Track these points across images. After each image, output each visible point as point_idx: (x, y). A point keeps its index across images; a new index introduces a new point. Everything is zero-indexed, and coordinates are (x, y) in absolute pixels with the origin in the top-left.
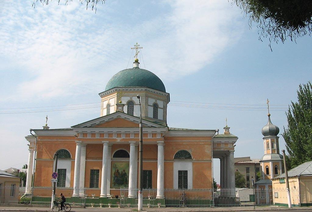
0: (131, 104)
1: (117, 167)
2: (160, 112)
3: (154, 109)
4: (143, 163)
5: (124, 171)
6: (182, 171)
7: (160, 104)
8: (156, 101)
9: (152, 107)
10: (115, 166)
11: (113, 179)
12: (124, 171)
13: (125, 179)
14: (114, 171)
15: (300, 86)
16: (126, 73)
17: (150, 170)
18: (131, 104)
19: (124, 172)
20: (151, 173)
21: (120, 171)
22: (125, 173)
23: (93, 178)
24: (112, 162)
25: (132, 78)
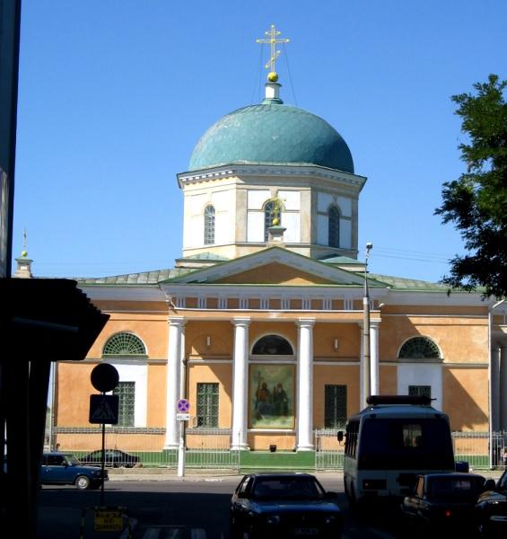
0: (271, 211)
1: (262, 376)
2: (344, 226)
3: (330, 219)
4: (154, 426)
5: (280, 386)
6: (417, 387)
7: (344, 206)
8: (335, 199)
9: (324, 217)
10: (257, 375)
11: (253, 406)
12: (280, 386)
13: (282, 405)
14: (255, 386)
15: (446, 221)
16: (257, 122)
17: (343, 384)
18: (271, 211)
19: (280, 390)
20: (345, 393)
21: (271, 387)
22: (283, 391)
23: (205, 407)
24: (250, 365)
25: (274, 138)
